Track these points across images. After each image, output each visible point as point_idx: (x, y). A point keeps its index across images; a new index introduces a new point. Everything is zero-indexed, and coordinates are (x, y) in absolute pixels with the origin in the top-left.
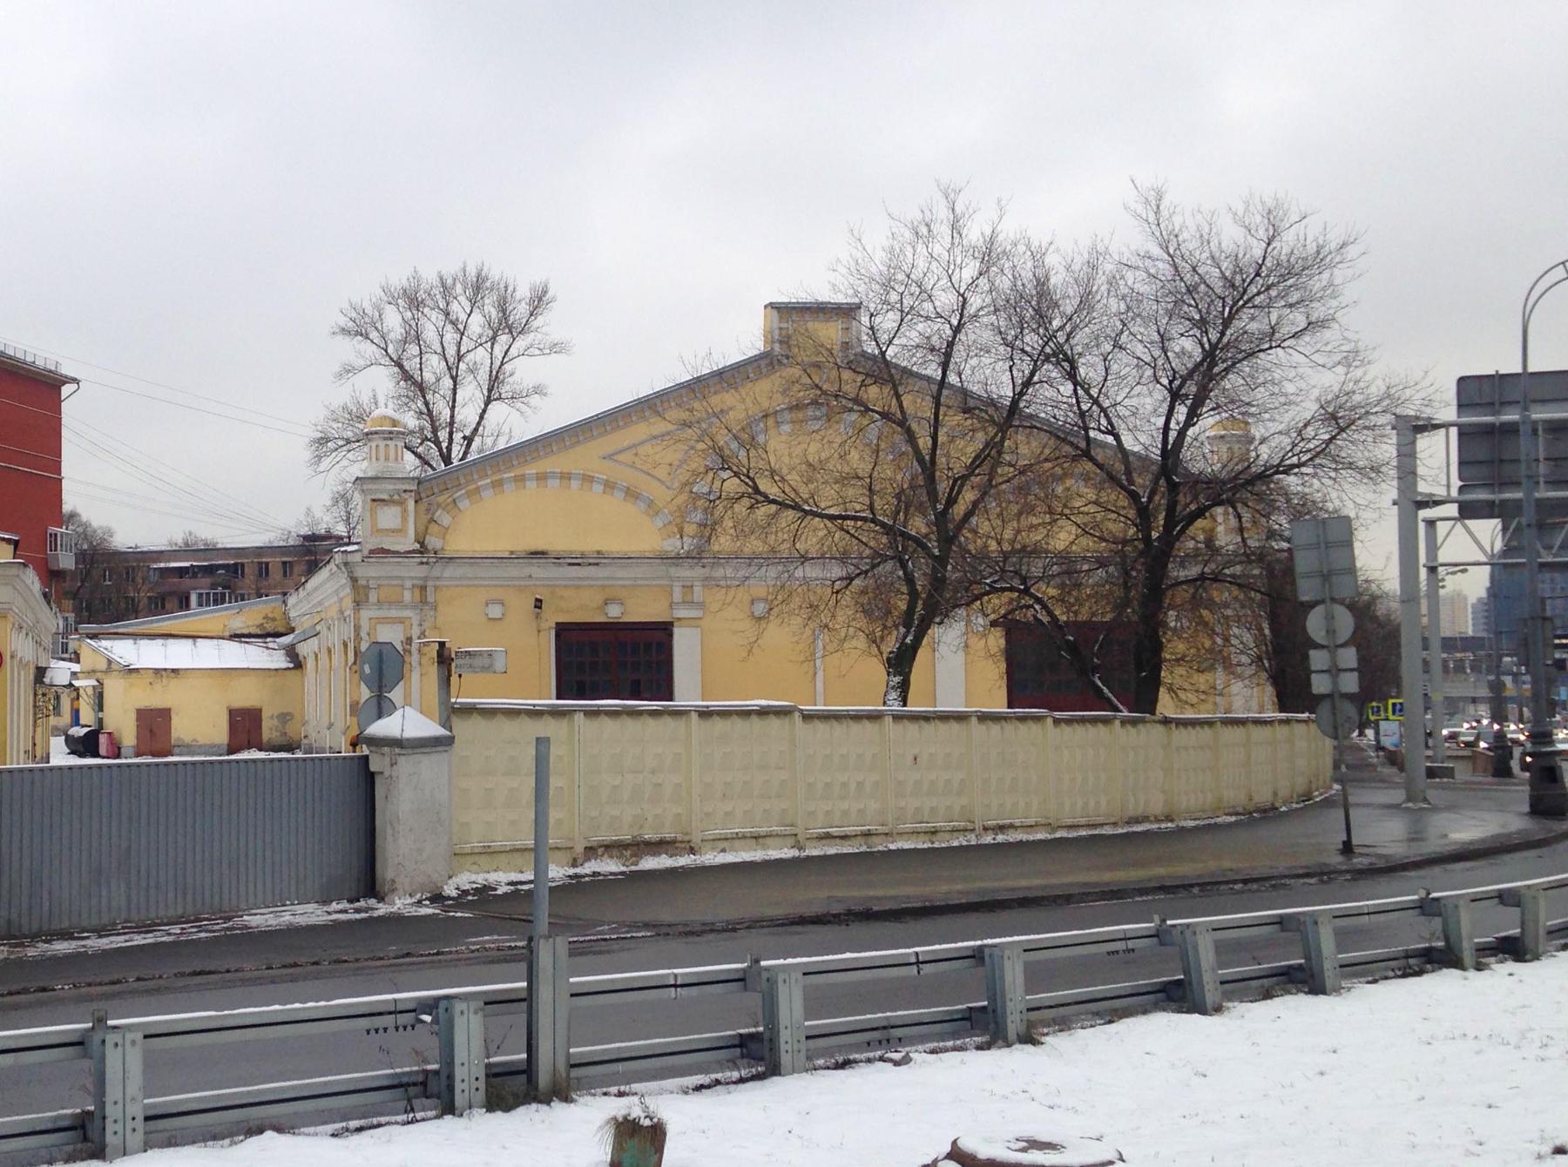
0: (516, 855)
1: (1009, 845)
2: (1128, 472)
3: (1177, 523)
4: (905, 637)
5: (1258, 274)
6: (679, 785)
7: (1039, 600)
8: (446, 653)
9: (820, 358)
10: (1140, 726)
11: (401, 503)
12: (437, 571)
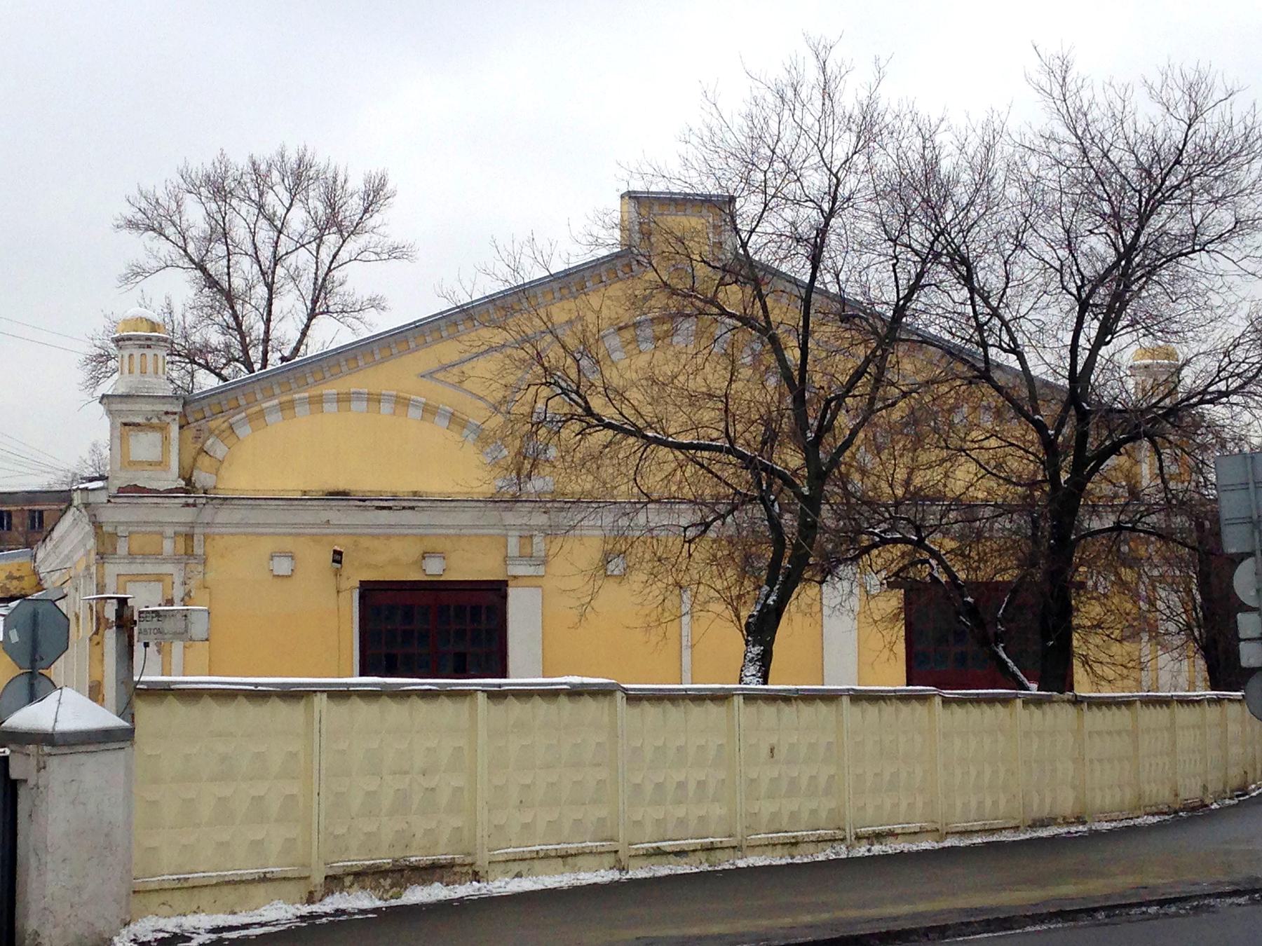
0: (226, 889)
1: (886, 857)
2: (1033, 397)
3: (1087, 465)
4: (768, 596)
5: (1178, 162)
6: (460, 789)
7: (934, 554)
8: (127, 613)
9: (679, 254)
10: (1046, 707)
11: (162, 428)
12: (208, 514)
